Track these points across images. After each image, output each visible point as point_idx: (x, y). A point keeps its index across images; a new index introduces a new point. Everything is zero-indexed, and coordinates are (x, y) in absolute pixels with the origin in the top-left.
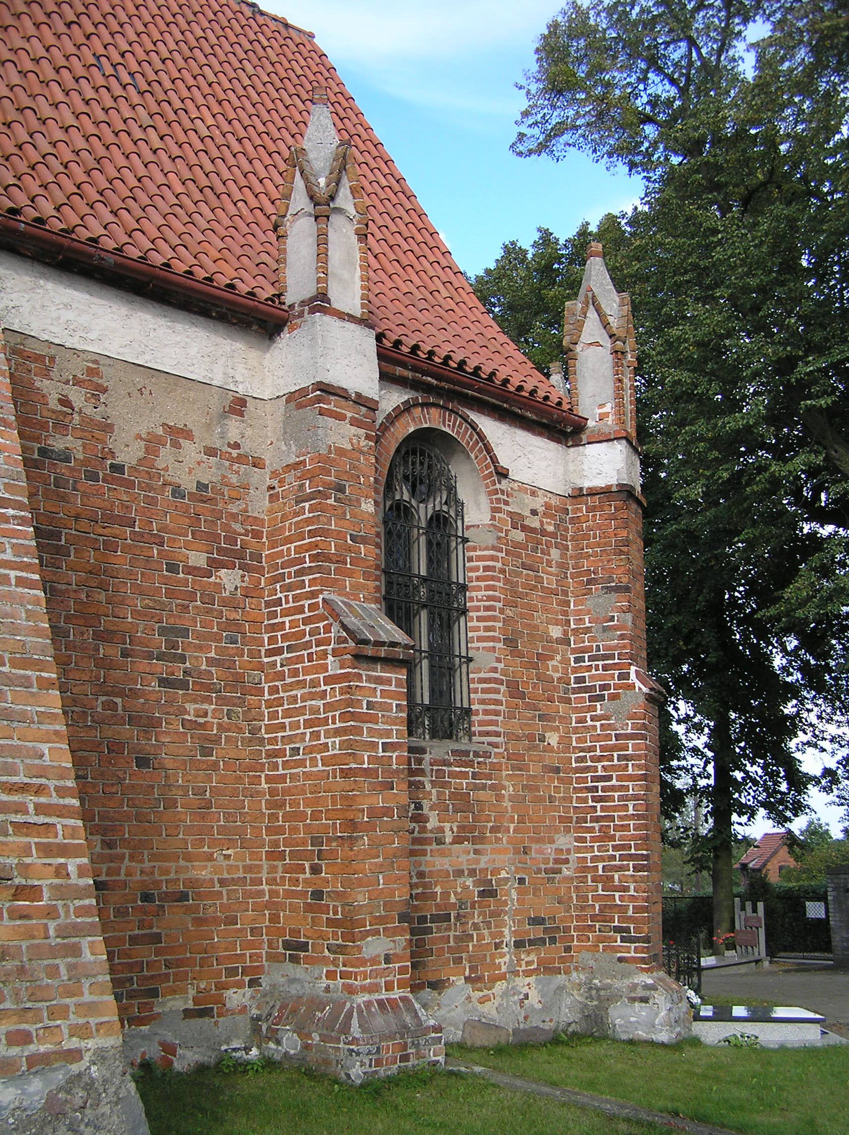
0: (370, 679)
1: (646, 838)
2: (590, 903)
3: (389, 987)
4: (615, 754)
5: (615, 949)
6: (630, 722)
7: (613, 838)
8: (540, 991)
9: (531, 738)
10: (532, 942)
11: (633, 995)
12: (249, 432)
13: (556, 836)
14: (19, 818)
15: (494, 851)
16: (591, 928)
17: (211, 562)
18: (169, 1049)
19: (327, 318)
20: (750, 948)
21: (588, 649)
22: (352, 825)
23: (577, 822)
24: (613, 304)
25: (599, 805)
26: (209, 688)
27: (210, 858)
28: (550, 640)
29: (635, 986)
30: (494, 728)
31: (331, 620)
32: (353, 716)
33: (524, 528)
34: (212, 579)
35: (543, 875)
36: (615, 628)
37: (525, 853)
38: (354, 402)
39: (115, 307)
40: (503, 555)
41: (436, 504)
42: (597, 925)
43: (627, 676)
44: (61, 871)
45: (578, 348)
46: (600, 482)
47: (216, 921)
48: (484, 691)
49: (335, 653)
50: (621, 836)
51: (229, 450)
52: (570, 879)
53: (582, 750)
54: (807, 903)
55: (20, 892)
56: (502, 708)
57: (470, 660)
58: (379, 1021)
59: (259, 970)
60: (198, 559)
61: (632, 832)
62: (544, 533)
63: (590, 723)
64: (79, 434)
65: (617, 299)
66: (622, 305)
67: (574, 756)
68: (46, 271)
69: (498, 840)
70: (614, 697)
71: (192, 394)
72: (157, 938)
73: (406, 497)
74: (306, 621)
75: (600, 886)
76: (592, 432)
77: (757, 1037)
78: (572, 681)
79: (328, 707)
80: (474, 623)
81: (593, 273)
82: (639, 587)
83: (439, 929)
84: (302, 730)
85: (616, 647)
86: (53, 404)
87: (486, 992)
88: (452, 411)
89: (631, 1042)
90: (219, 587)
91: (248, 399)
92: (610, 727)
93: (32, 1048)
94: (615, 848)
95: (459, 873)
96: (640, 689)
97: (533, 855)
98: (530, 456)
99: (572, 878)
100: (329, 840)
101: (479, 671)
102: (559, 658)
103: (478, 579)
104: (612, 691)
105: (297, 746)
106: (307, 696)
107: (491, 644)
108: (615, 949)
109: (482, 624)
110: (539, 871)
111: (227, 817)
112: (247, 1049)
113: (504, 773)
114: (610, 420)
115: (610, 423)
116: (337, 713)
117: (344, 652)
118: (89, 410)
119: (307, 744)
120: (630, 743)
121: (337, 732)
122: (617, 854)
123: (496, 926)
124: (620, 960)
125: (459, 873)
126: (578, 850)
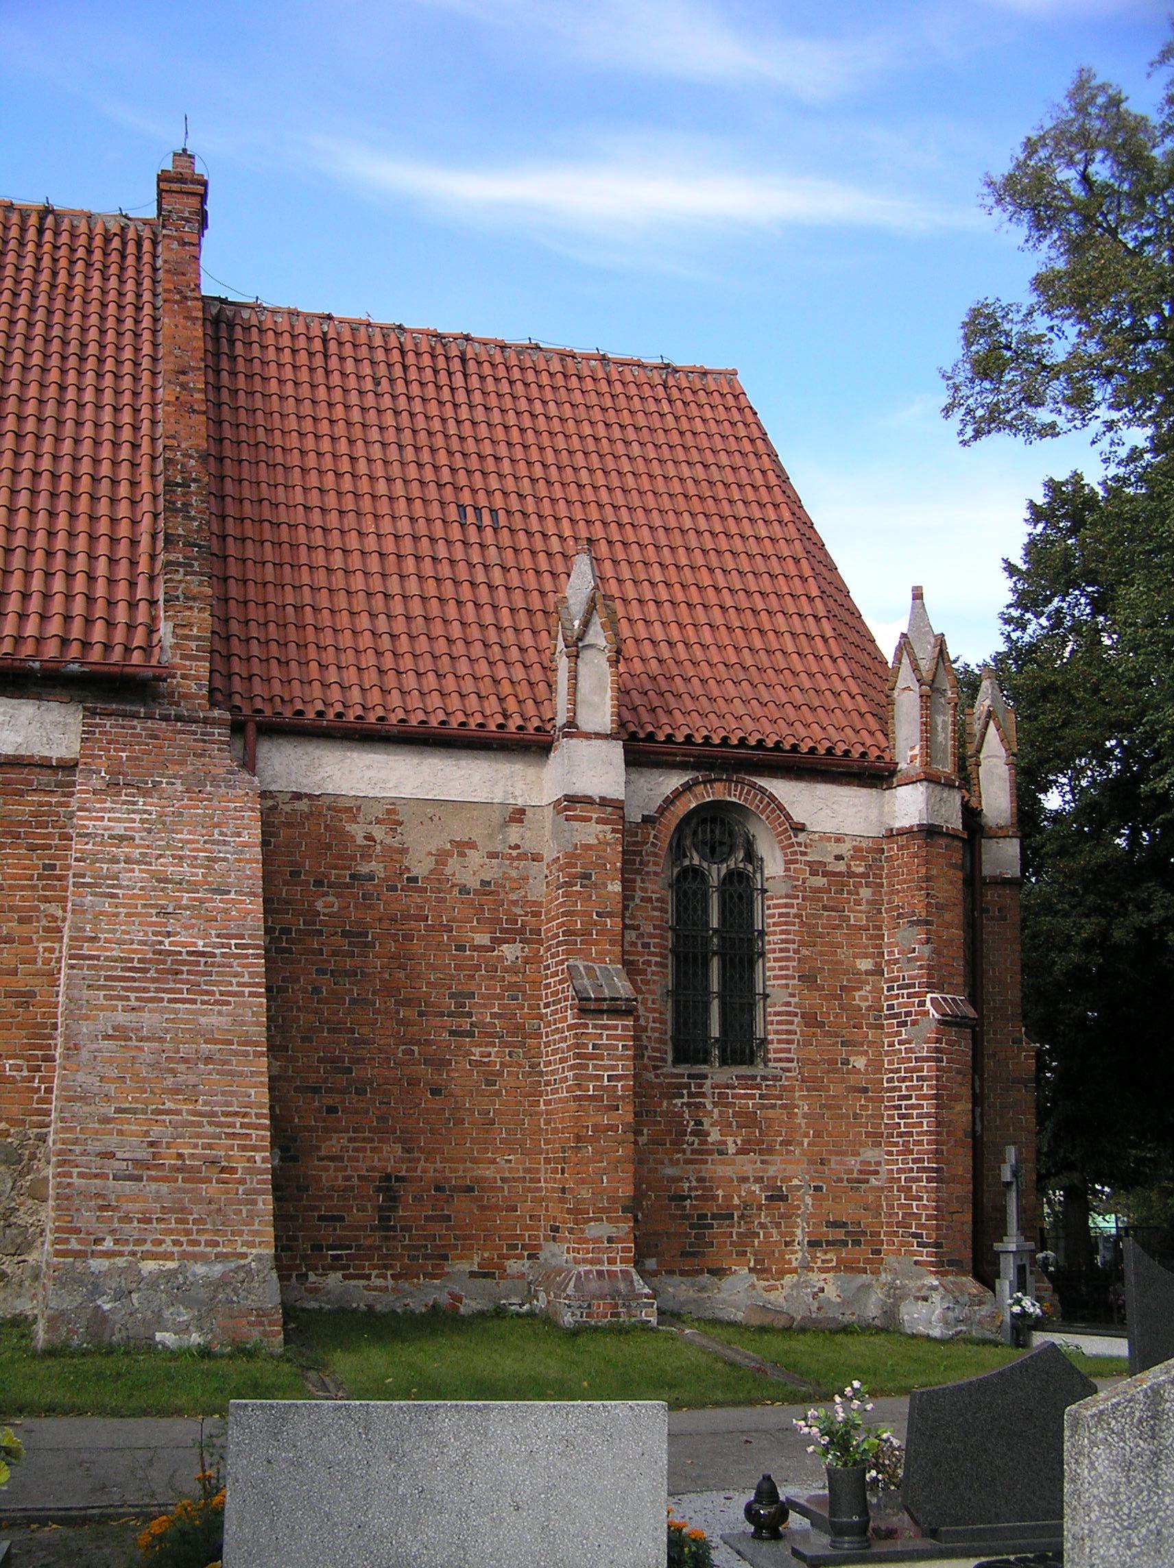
0: (595, 1027)
3: (611, 1261)
5: (914, 1253)
7: (911, 1152)
9: (832, 1062)
12: (528, 834)
14: (230, 1130)
15: (783, 1162)
17: (493, 940)
18: (457, 1298)
19: (574, 741)
21: (896, 979)
25: (902, 1122)
26: (491, 1035)
27: (493, 1161)
28: (859, 973)
33: (825, 874)
34: (495, 953)
36: (916, 959)
39: (408, 759)
40: (800, 901)
41: (736, 861)
44: (251, 1160)
45: (896, 693)
46: (905, 822)
47: (497, 1208)
53: (892, 1071)
55: (223, 1170)
57: (768, 996)
59: (539, 1247)
60: (483, 939)
62: (851, 874)
63: (897, 1046)
64: (382, 859)
68: (353, 745)
69: (789, 1152)
70: (914, 1023)
71: (475, 813)
72: (448, 1218)
73: (696, 861)
80: (772, 964)
83: (720, 1226)
86: (360, 840)
87: (773, 1282)
90: (502, 958)
93: (219, 1249)
94: (914, 1161)
95: (745, 1179)
97: (833, 1166)
98: (835, 806)
103: (775, 924)
107: (784, 982)
108: (914, 1253)
109: (777, 964)
110: (841, 1180)
111: (508, 1131)
112: (521, 1305)
113: (797, 1094)
114: (917, 762)
118: (388, 841)
120: (926, 1065)
121: (572, 1068)
122: (915, 1166)
124: (916, 1263)
125: (745, 1179)
126: (888, 1162)
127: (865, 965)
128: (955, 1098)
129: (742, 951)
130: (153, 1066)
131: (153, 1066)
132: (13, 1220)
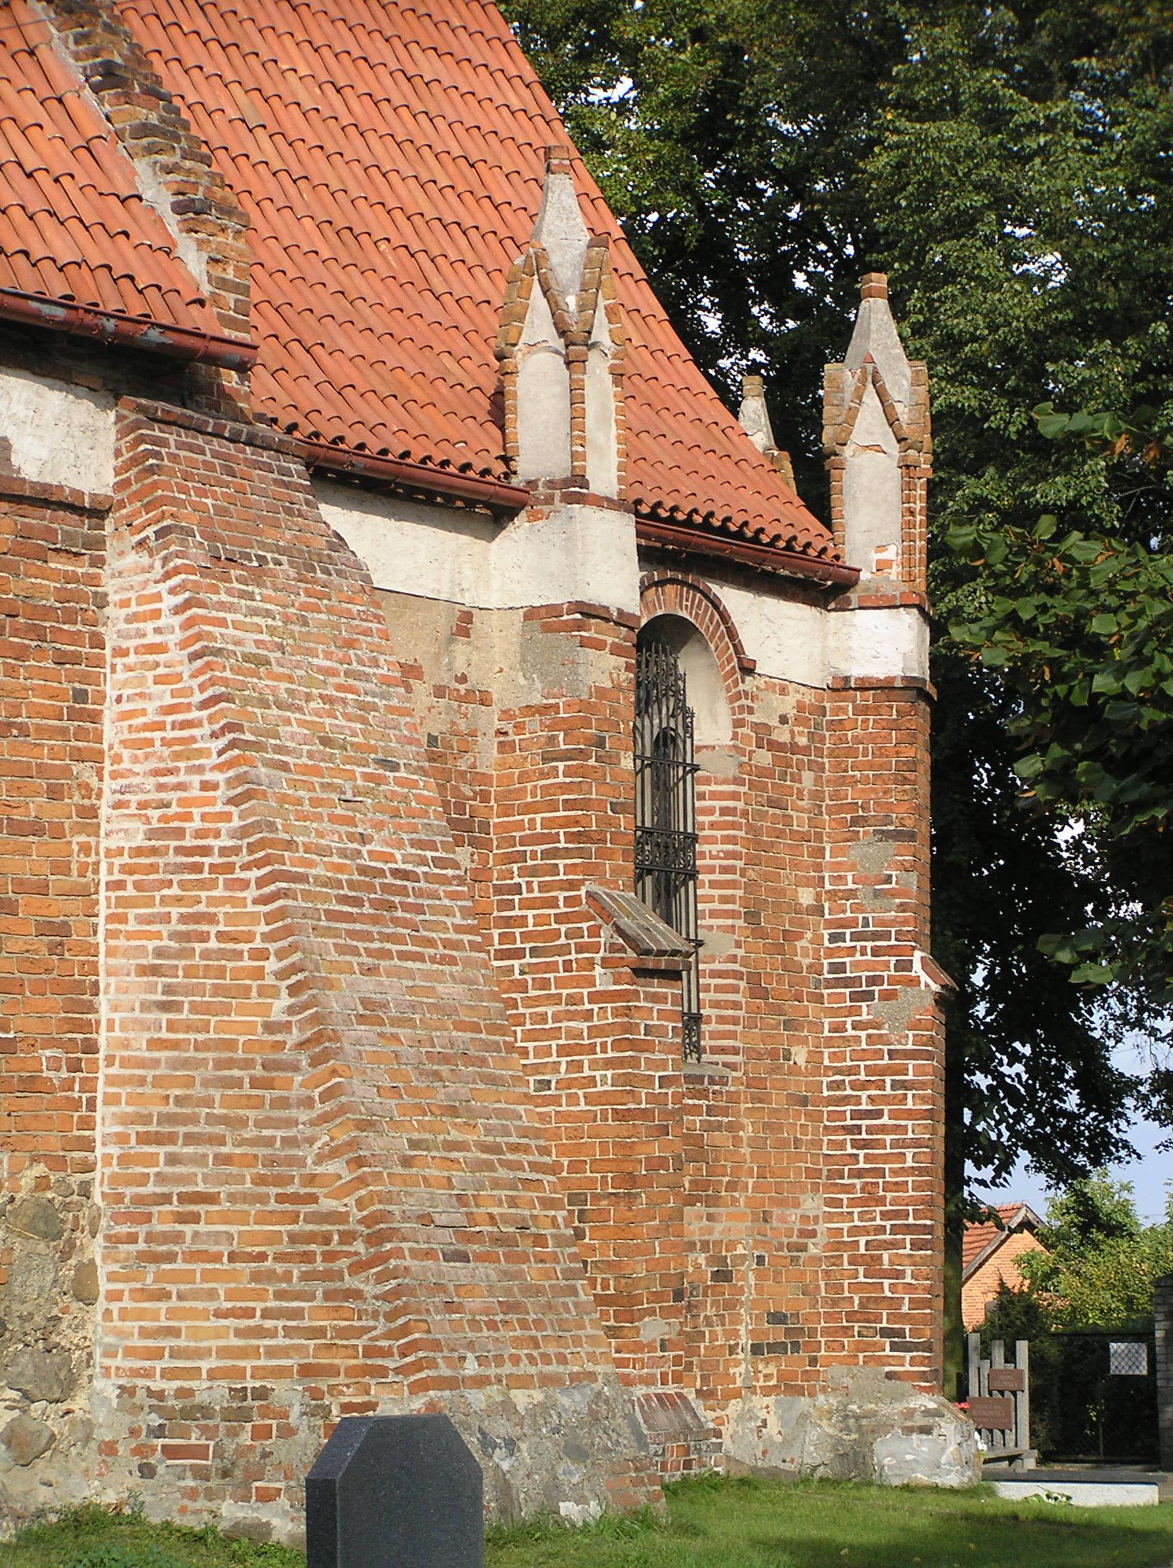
1: (930, 1202)
2: (847, 1294)
4: (888, 1079)
5: (882, 1361)
6: (910, 1033)
7: (881, 1201)
8: (781, 1418)
9: (774, 1055)
10: (772, 1348)
11: (909, 1424)
12: (475, 658)
13: (802, 1197)
15: (730, 1217)
16: (847, 1331)
20: (997, 1433)
21: (852, 923)
22: (631, 1179)
23: (828, 1178)
24: (904, 380)
25: (861, 1153)
29: (910, 1413)
30: (731, 1043)
31: (600, 921)
32: (633, 1045)
33: (773, 746)
35: (785, 1253)
36: (893, 894)
37: (765, 1220)
38: (616, 623)
42: (856, 1325)
43: (908, 966)
45: (847, 451)
46: (878, 670)
48: (719, 989)
49: (605, 963)
50: (894, 1199)
51: (457, 686)
52: (817, 1260)
53: (839, 1071)
54: (1114, 1346)
56: (741, 1013)
58: (661, 1418)
61: (911, 1193)
63: (850, 1032)
65: (908, 372)
66: (915, 383)
67: (825, 1080)
70: (887, 996)
71: (420, 616)
74: (560, 919)
75: (861, 1270)
76: (867, 589)
77: (1069, 1498)
78: (826, 968)
79: (594, 1031)
81: (873, 327)
82: (925, 830)
84: (554, 1058)
85: (893, 922)
87: (719, 1413)
88: (696, 589)
89: (906, 1488)
91: (474, 611)
92: (881, 1039)
94: (885, 1215)
96: (927, 985)
97: (775, 1224)
99: (820, 1259)
100: (596, 1198)
101: (712, 959)
102: (809, 935)
103: (712, 826)
104: (885, 986)
105: (547, 1077)
106: (562, 1016)
107: (730, 922)
108: (882, 1361)
109: (716, 892)
113: (743, 1106)
114: (894, 573)
115: (893, 577)
116: (609, 1040)
117: (621, 962)
119: (562, 1076)
121: (609, 1064)
122: (888, 1224)
123: (731, 1323)
124: (889, 1376)
126: (829, 1217)
132: (55, 1338)
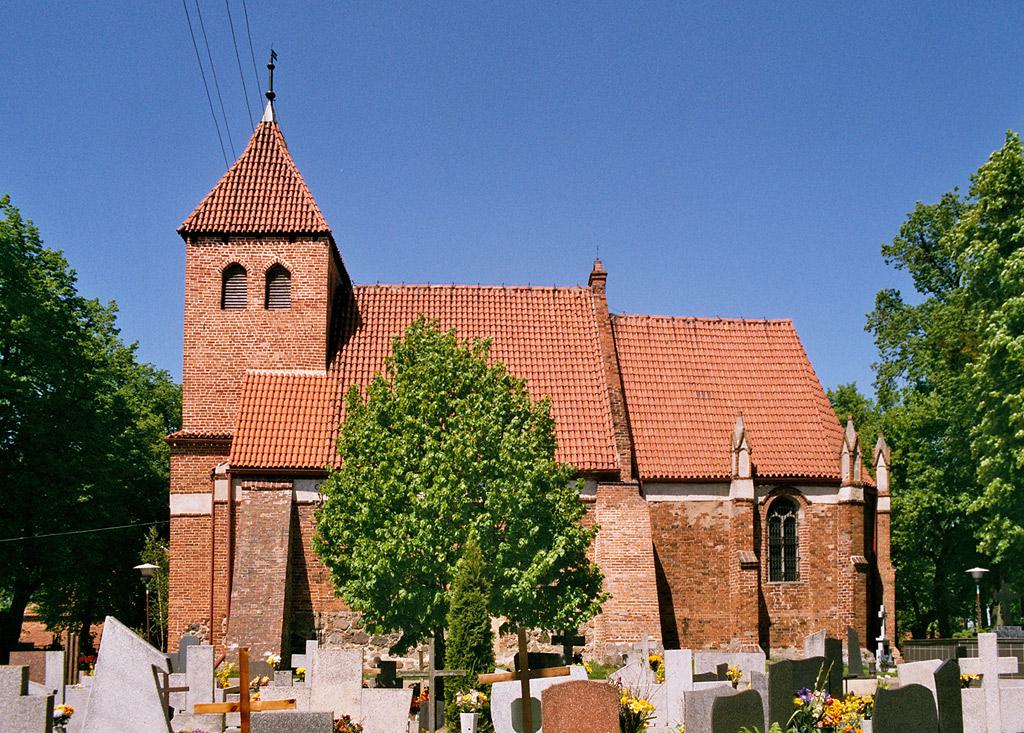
60: (711, 544)
127: (831, 547)
128: (861, 590)
129: (791, 548)
130: (627, 589)
131: (627, 589)
